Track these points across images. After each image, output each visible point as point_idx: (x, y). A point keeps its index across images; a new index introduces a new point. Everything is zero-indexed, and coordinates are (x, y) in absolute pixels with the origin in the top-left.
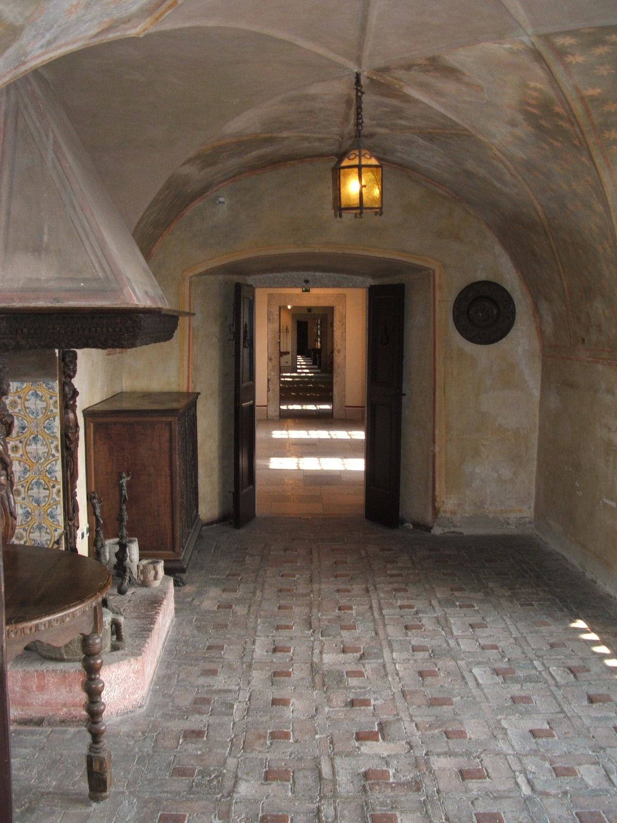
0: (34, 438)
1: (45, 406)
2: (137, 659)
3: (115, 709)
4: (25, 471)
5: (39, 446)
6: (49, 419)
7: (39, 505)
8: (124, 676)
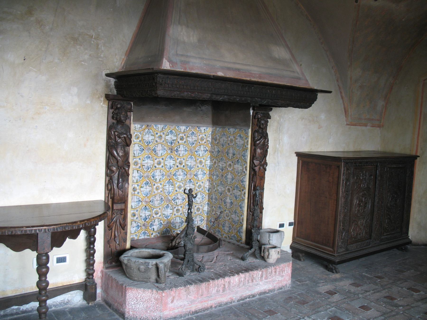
0: (238, 160)
1: (243, 143)
2: (158, 292)
3: (139, 316)
4: (233, 179)
5: (239, 166)
6: (244, 151)
7: (236, 199)
8: (147, 298)
